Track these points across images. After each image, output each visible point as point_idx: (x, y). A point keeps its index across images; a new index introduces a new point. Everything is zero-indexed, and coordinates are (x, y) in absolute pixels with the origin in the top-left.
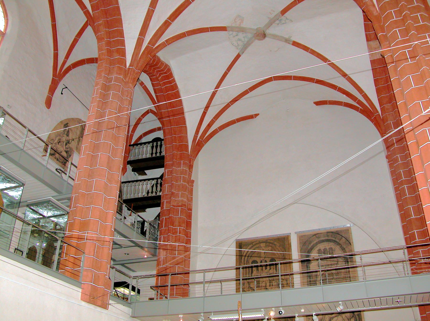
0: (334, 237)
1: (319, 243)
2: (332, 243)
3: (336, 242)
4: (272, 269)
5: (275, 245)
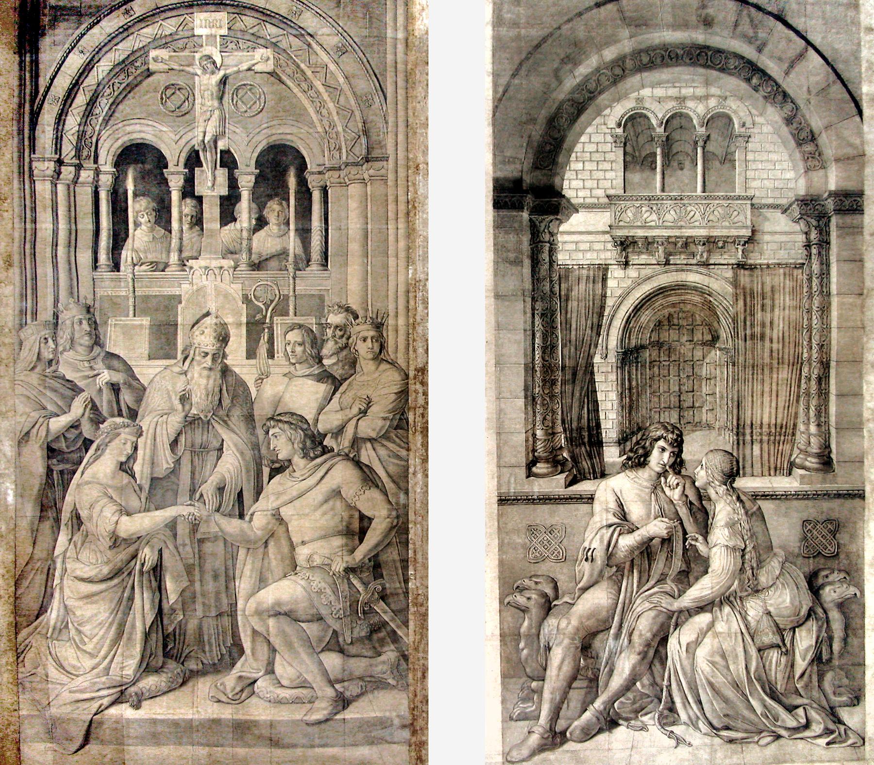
0: (750, 40)
1: (642, 68)
2: (733, 83)
3: (764, 74)
4: (273, 227)
5: (302, 33)
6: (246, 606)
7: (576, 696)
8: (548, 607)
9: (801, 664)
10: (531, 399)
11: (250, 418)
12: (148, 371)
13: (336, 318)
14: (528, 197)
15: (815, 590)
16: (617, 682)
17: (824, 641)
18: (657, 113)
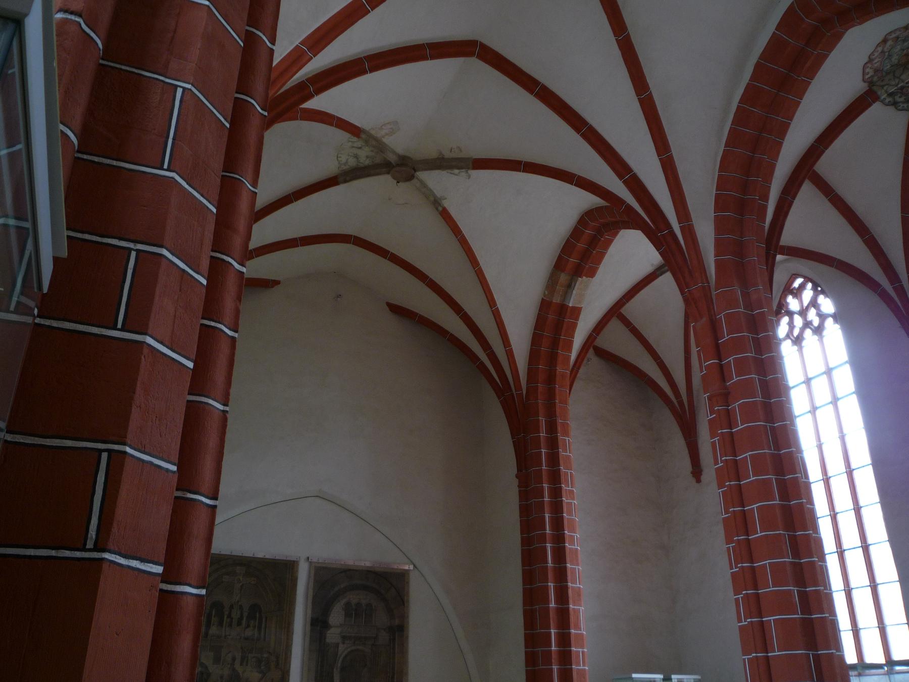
13: (265, 655)
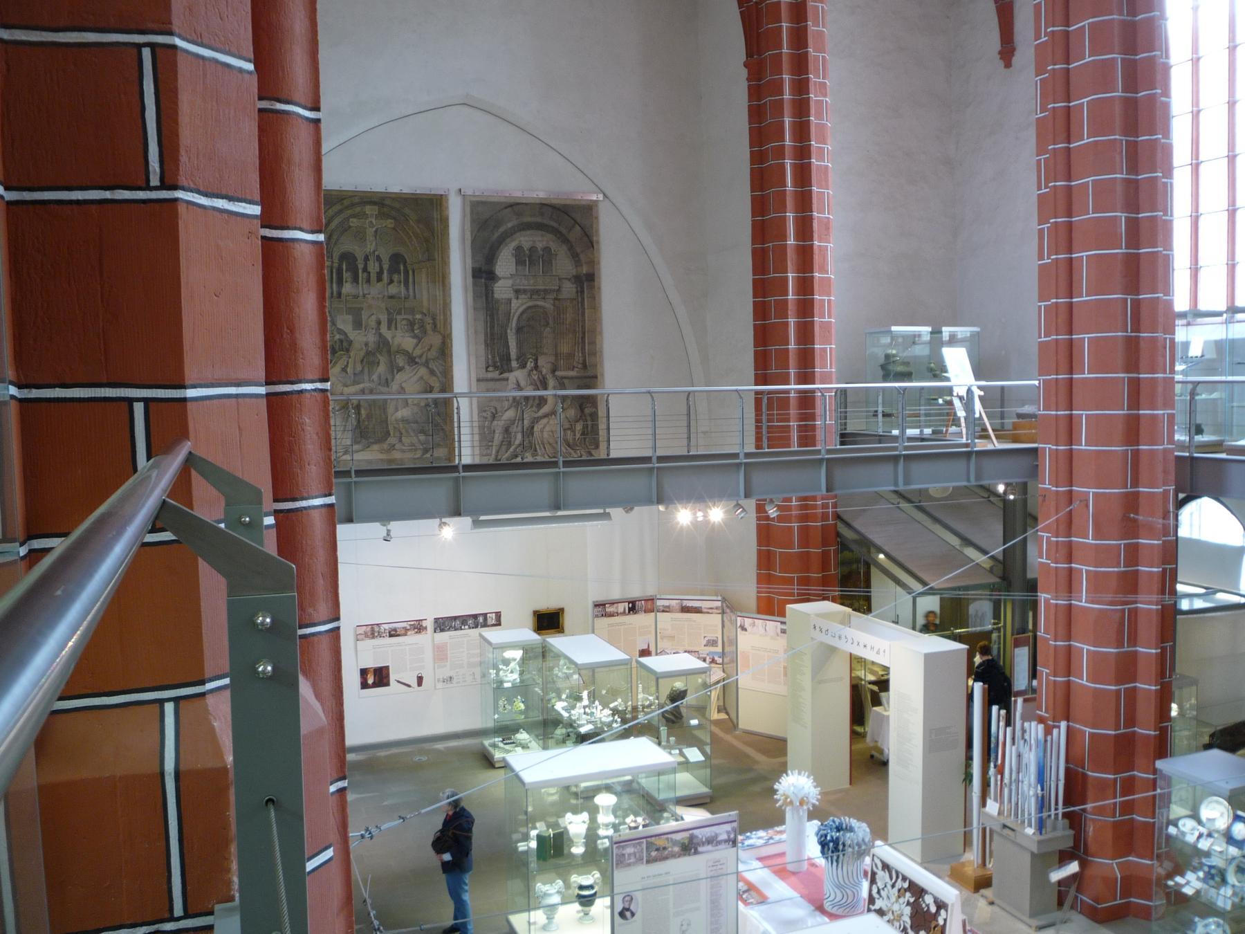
6: (391, 419)
7: (504, 448)
8: (494, 417)
9: (578, 436)
10: (487, 345)
11: (389, 352)
12: (353, 335)
13: (418, 316)
14: (483, 275)
15: (582, 410)
16: (517, 442)
17: (585, 427)
18: (526, 246)
